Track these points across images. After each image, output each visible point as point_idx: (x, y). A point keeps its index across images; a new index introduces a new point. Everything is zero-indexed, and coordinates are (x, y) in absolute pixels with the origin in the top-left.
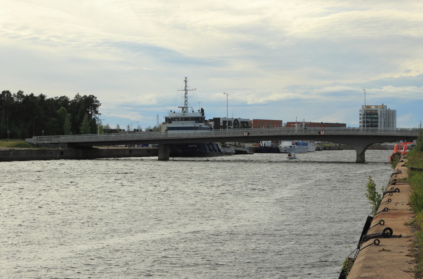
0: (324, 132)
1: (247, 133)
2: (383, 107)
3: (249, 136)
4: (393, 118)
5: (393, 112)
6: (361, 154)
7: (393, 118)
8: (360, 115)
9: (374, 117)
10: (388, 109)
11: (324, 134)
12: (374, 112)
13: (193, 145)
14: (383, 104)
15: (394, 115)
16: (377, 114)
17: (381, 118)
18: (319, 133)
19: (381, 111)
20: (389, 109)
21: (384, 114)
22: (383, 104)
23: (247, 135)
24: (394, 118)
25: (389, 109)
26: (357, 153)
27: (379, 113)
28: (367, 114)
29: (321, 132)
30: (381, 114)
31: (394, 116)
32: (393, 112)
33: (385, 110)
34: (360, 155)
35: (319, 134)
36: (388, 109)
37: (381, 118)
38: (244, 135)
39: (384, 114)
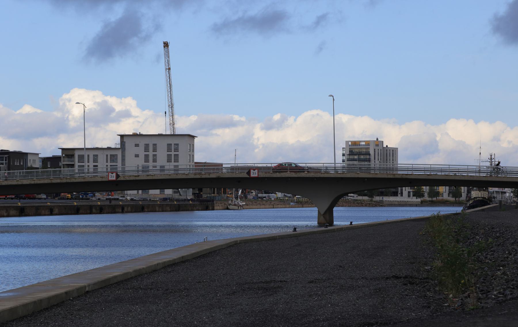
0: (256, 171)
1: (114, 174)
2: (378, 143)
3: (119, 179)
4: (393, 160)
5: (393, 150)
6: (325, 213)
7: (393, 160)
8: (343, 155)
9: (367, 159)
10: (385, 146)
11: (256, 175)
12: (364, 151)
13: (18, 164)
14: (377, 139)
15: (394, 155)
16: (370, 155)
17: (375, 160)
18: (249, 173)
19: (375, 149)
20: (387, 146)
21: (380, 154)
22: (377, 139)
23: (114, 179)
24: (394, 160)
25: (387, 146)
26: (318, 210)
27: (372, 152)
28: (351, 153)
29: (252, 171)
30: (375, 154)
31: (394, 157)
32: (393, 150)
33: (380, 148)
34: (324, 214)
35: (247, 176)
36: (385, 146)
37: (375, 160)
38: (110, 179)
39: (380, 154)
